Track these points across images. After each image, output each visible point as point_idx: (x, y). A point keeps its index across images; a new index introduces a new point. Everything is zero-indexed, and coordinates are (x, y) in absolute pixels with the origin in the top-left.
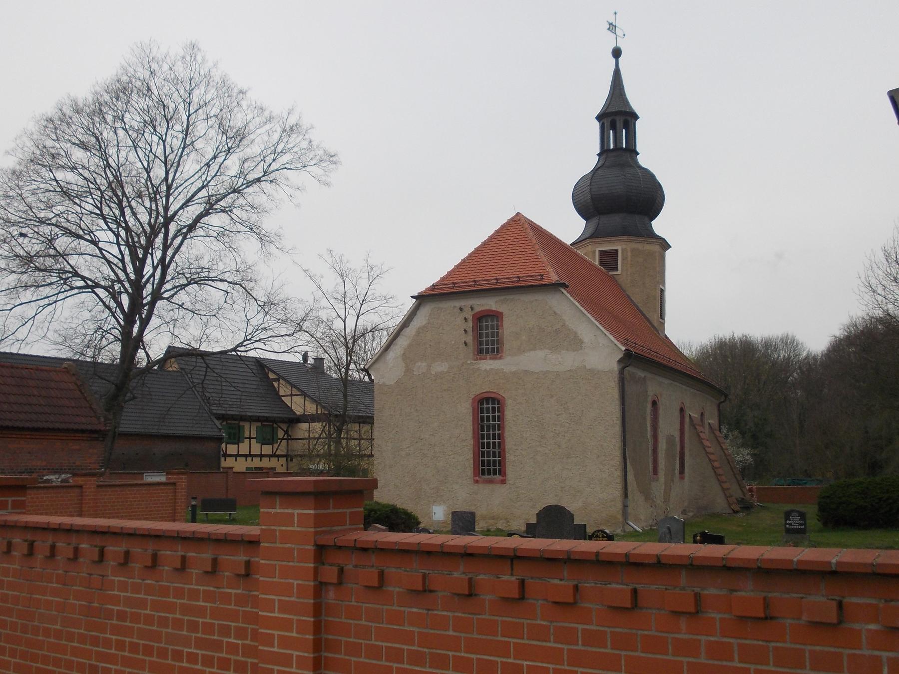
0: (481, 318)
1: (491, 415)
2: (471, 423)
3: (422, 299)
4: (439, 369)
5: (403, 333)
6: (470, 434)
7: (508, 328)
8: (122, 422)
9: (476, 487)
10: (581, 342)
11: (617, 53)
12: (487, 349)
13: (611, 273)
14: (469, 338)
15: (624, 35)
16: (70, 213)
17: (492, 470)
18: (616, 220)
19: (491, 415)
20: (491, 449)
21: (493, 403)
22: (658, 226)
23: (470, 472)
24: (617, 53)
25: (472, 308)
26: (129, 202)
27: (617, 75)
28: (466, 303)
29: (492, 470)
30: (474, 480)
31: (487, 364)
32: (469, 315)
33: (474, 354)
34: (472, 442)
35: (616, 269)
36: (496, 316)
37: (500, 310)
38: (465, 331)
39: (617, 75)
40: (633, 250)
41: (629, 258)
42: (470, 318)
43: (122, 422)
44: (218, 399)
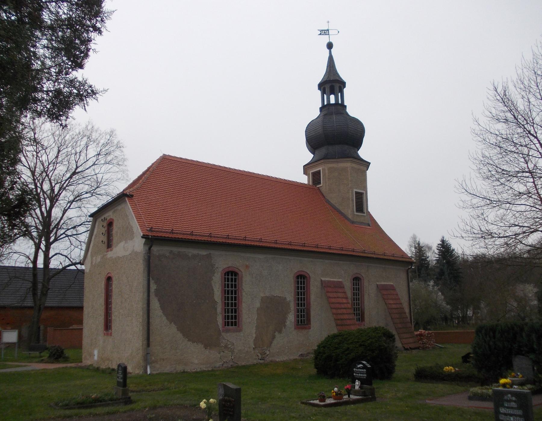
1: (230, 296)
8: (42, 278)
11: (330, 46)
12: (232, 322)
13: (318, 186)
15: (339, 32)
16: (495, 144)
17: (230, 303)
18: (337, 148)
19: (230, 302)
20: (230, 288)
22: (363, 153)
24: (330, 46)
26: (39, 158)
27: (331, 60)
29: (230, 303)
35: (320, 183)
39: (331, 60)
40: (329, 169)
41: (327, 174)
43: (42, 278)
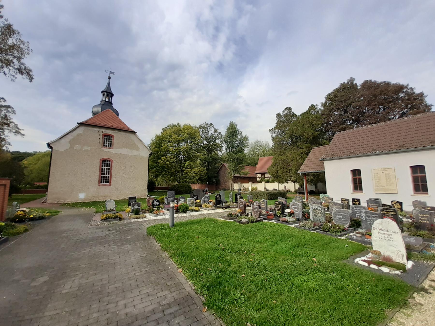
0: (105, 136)
2: (99, 167)
3: (81, 124)
4: (86, 149)
5: (69, 134)
6: (98, 170)
7: (115, 141)
9: (99, 187)
10: (139, 148)
14: (101, 141)
21: (107, 161)
23: (97, 182)
25: (103, 132)
27: (109, 83)
28: (102, 130)
30: (372, 245)
31: (107, 150)
32: (101, 134)
33: (102, 146)
34: (99, 173)
36: (111, 136)
37: (113, 135)
38: (99, 138)
39: (109, 83)
42: (101, 135)
44: (279, 209)
